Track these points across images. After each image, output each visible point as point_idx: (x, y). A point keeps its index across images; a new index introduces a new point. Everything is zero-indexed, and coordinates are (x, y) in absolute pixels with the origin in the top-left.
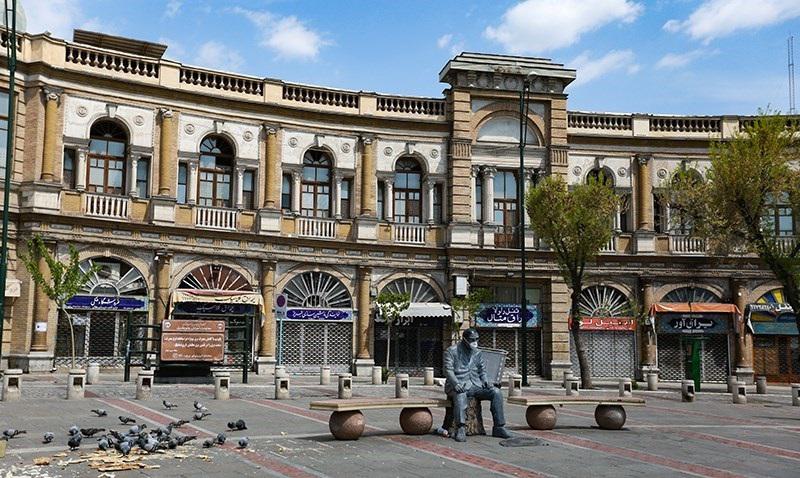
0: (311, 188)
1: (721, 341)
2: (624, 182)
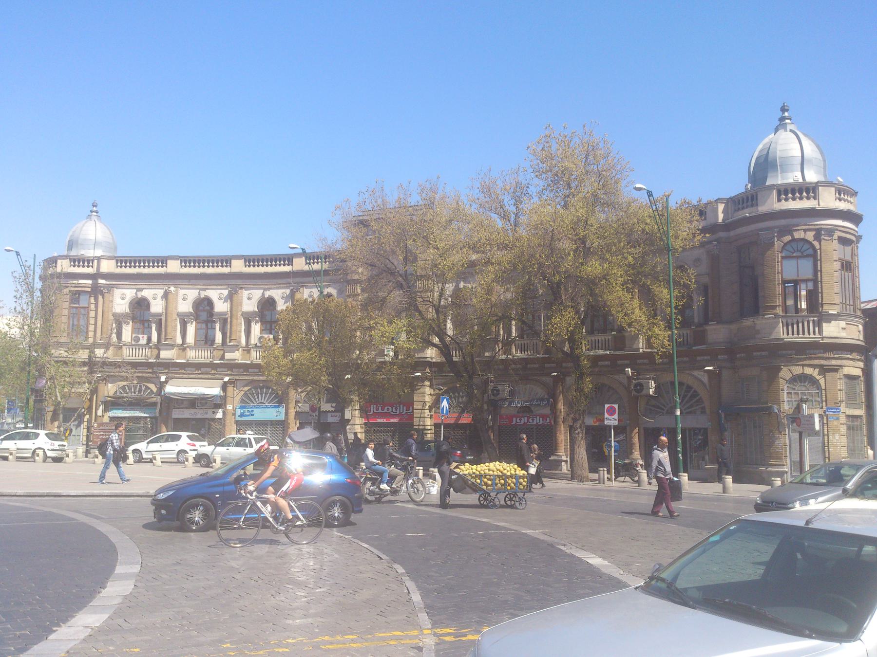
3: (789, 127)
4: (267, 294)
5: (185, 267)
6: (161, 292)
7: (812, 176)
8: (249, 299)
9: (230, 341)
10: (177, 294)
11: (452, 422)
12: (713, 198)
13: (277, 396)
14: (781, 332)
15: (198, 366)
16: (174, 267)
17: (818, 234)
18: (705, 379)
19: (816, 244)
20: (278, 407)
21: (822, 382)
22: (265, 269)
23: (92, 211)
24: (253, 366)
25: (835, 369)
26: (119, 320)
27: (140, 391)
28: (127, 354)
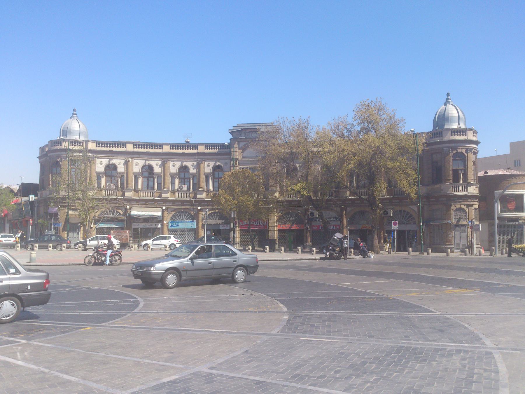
0: (217, 180)
1: (336, 321)
2: (193, 171)
3: (451, 103)
4: (184, 164)
5: (136, 148)
6: (123, 161)
7: (463, 126)
8: (173, 166)
9: (127, 186)
10: (132, 163)
11: (288, 228)
12: (420, 131)
13: (191, 216)
14: (452, 191)
15: (147, 201)
16: (130, 148)
17: (467, 150)
18: (416, 209)
19: (466, 154)
20: (192, 222)
21: (467, 211)
22: (184, 150)
23: (73, 114)
24: (176, 201)
25: (472, 206)
26: (99, 176)
27: (113, 214)
28: (104, 194)
